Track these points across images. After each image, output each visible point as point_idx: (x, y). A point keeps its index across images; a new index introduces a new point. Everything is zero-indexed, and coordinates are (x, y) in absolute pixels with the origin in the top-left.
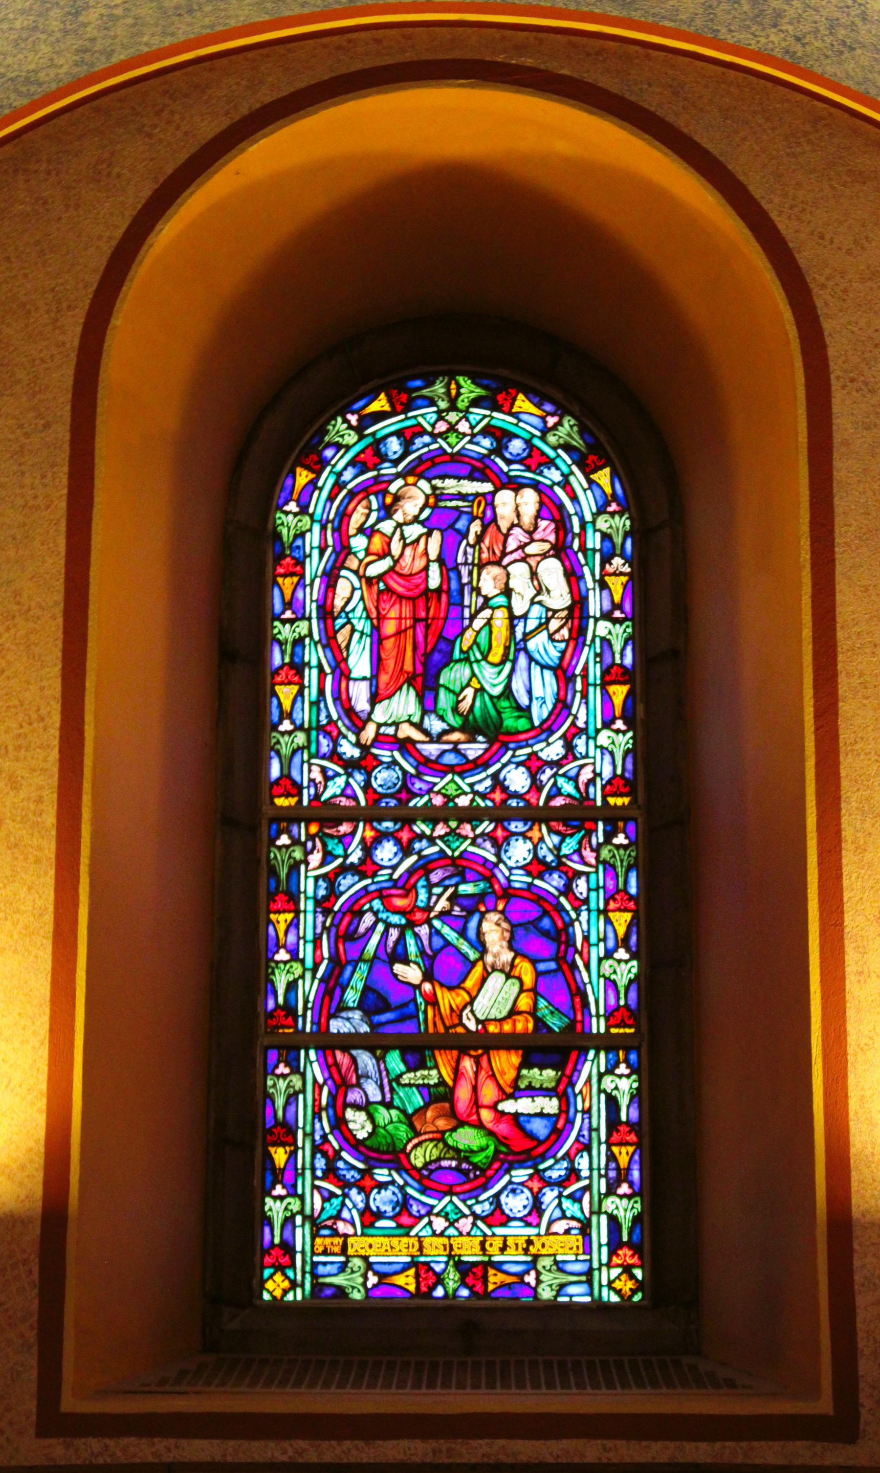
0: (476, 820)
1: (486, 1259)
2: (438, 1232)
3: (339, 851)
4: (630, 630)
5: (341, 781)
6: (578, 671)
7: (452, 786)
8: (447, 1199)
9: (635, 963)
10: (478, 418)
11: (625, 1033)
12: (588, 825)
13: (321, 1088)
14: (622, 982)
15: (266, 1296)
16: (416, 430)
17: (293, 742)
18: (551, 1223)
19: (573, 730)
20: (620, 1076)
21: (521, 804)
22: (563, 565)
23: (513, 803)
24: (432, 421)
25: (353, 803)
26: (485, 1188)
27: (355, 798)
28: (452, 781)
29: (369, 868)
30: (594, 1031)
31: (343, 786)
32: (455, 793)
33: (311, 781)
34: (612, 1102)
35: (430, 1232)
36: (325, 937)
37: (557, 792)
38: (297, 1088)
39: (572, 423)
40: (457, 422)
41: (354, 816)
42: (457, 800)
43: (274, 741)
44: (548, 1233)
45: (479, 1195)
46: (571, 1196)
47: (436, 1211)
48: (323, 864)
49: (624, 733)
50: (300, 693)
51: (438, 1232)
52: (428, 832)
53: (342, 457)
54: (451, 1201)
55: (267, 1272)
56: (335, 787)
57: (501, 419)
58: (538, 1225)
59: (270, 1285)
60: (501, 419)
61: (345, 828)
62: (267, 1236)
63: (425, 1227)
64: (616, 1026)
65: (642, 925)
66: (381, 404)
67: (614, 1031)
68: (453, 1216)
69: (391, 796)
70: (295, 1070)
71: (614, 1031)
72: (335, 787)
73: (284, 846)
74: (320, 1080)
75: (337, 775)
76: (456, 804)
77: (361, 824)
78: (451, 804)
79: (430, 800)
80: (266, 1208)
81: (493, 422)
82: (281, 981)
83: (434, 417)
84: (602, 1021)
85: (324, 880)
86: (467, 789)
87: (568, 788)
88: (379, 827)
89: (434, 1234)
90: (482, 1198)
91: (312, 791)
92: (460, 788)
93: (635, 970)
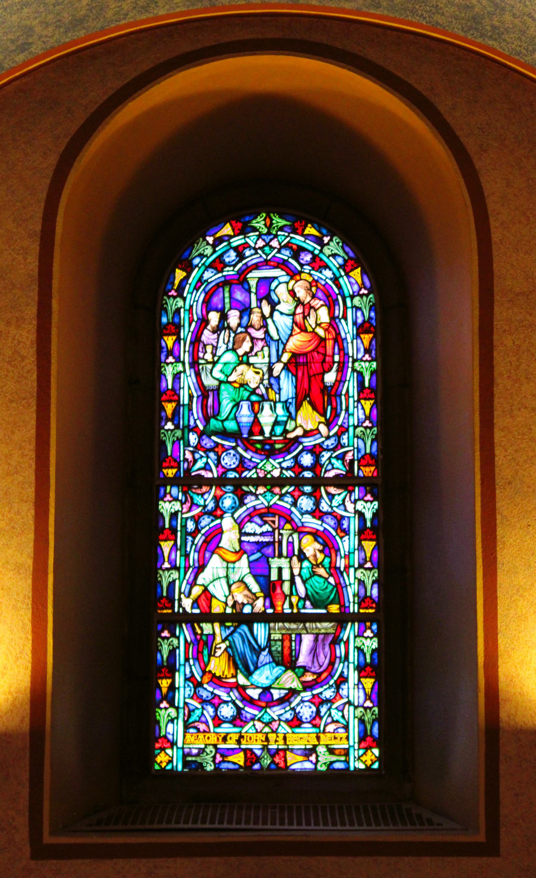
0: (254, 479)
1: (286, 747)
2: (259, 730)
4: (376, 575)
6: (344, 392)
8: (271, 503)
9: (376, 503)
10: (283, 238)
11: (369, 613)
12: (350, 488)
13: (189, 644)
14: (369, 516)
15: (157, 767)
16: (246, 246)
17: (170, 576)
18: (326, 725)
20: (366, 638)
22: (337, 377)
24: (254, 241)
26: (290, 453)
27: (328, 494)
28: (267, 255)
29: (219, 513)
30: (351, 611)
31: (200, 715)
32: (271, 469)
33: (186, 460)
34: (360, 375)
35: (254, 731)
38: (173, 717)
39: (337, 241)
41: (210, 482)
42: (272, 473)
43: (164, 302)
44: (324, 732)
45: (285, 456)
47: (276, 250)
49: (372, 502)
50: (175, 544)
51: (259, 730)
57: (298, 240)
59: (159, 759)
60: (298, 240)
61: (204, 489)
62: (164, 385)
63: (283, 241)
64: (364, 608)
65: (379, 404)
66: (227, 230)
67: (362, 611)
69: (234, 470)
70: (173, 635)
71: (362, 611)
73: (169, 430)
74: (189, 640)
77: (214, 488)
78: (269, 487)
80: (160, 507)
81: (293, 241)
82: (169, 372)
83: (256, 238)
84: (356, 606)
85: (191, 520)
86: (278, 466)
89: (257, 732)
90: (286, 458)
91: (186, 466)
92: (273, 466)
93: (376, 507)
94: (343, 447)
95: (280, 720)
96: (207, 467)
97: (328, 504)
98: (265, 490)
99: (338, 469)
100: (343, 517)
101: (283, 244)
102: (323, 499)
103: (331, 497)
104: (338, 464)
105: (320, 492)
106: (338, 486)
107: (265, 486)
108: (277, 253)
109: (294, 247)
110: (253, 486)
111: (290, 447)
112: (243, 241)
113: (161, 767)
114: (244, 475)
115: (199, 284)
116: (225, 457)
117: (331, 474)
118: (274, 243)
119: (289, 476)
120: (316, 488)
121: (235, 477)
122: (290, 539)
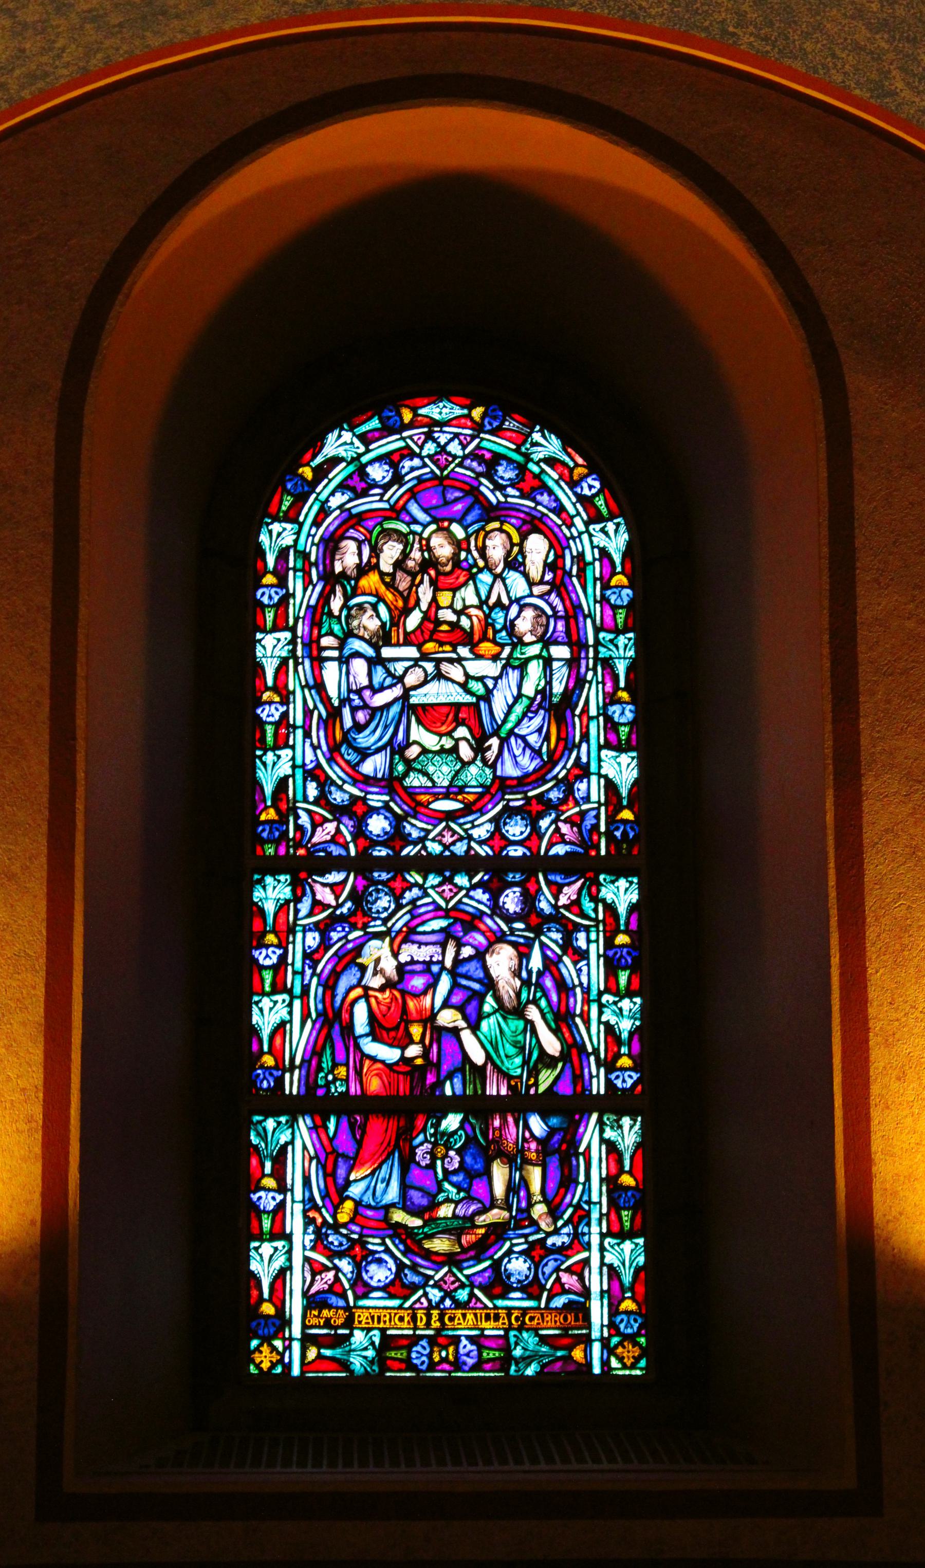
3: (565, 828)
5: (331, 827)
6: (309, 1024)
7: (448, 894)
14: (622, 910)
16: (405, 452)
19: (316, 956)
21: (376, 874)
23: (384, 876)
24: (420, 442)
25: (550, 877)
27: (549, 883)
30: (595, 1092)
36: (577, 739)
37: (336, 888)
40: (447, 444)
46: (569, 1270)
48: (311, 914)
52: (420, 881)
53: (325, 487)
54: (447, 902)
55: (254, 1343)
56: (568, 894)
58: (539, 1299)
68: (446, 888)
69: (384, 844)
72: (568, 894)
75: (326, 820)
76: (451, 852)
79: (470, 880)
81: (485, 444)
86: (430, 891)
87: (325, 895)
88: (525, 851)
94: (317, 925)
95: (470, 838)
96: (336, 838)
97: (551, 904)
98: (452, 848)
99: (324, 885)
100: (316, 802)
101: (421, 1292)
102: (543, 894)
103: (557, 890)
104: (325, 895)
105: (538, 882)
106: (567, 873)
107: (439, 873)
108: (457, 465)
109: (488, 455)
110: (418, 872)
111: (633, 563)
112: (401, 444)
113: (261, 1369)
114: (404, 852)
115: (322, 516)
116: (333, 796)
117: (334, 877)
118: (435, 1294)
119: (484, 854)
120: (363, 854)
121: (388, 854)
122: (314, 530)
